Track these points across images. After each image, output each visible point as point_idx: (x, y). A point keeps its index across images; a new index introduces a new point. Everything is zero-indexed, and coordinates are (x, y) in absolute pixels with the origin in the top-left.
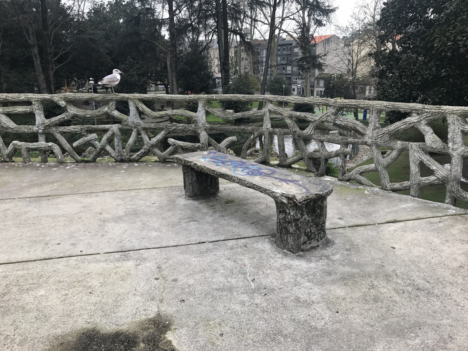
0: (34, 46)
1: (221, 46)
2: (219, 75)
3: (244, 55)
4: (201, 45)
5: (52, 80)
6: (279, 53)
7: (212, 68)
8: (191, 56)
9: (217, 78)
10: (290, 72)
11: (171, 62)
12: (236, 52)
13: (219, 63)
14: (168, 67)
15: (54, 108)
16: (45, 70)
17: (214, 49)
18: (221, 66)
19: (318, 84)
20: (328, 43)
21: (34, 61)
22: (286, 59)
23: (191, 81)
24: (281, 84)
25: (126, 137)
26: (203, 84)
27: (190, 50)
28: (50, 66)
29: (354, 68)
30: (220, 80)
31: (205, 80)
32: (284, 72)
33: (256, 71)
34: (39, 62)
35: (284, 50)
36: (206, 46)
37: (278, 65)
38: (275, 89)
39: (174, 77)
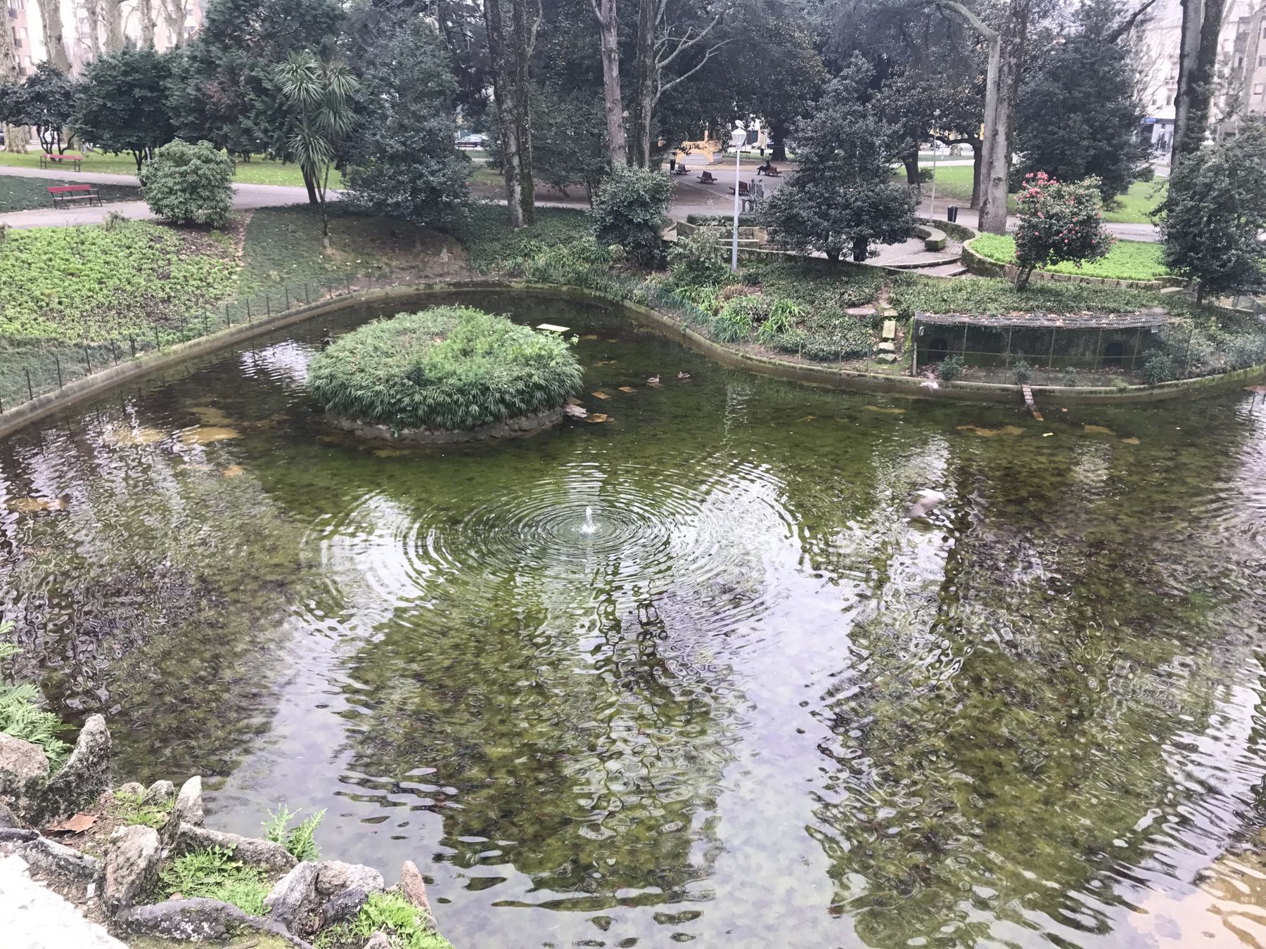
0: (607, 27)
2: (1170, 113)
4: (1119, 12)
5: (647, 122)
7: (1144, 89)
8: (1076, 50)
11: (1000, 70)
12: (1241, 38)
13: (1176, 74)
14: (989, 85)
15: (630, 204)
16: (632, 101)
17: (1162, 29)
18: (1179, 82)
23: (1061, 133)
25: (809, 308)
26: (1103, 144)
27: (1074, 29)
28: (649, 83)
31: (1111, 131)
34: (615, 73)
36: (1135, 15)
39: (1003, 118)
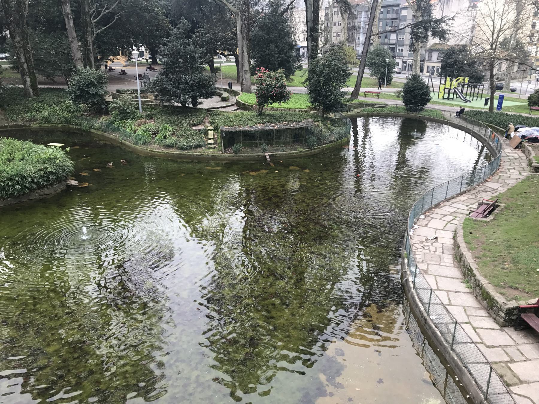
1: (308, 5)
2: (305, 44)
3: (337, 18)
4: (283, 4)
5: (91, 48)
6: (381, 16)
9: (302, 47)
10: (394, 42)
11: (242, 26)
12: (327, 15)
13: (306, 29)
14: (238, 32)
15: (88, 85)
16: (82, 37)
18: (307, 32)
19: (430, 57)
20: (447, 3)
21: (66, 22)
22: (390, 25)
23: (268, 51)
24: (384, 57)
25: (176, 128)
27: (267, 10)
28: (89, 29)
29: (495, 36)
30: (306, 49)
31: (285, 51)
32: (386, 41)
33: (351, 39)
34: (72, 24)
35: (388, 12)
36: (289, 5)
37: (380, 33)
38: (375, 64)
39: (245, 46)
